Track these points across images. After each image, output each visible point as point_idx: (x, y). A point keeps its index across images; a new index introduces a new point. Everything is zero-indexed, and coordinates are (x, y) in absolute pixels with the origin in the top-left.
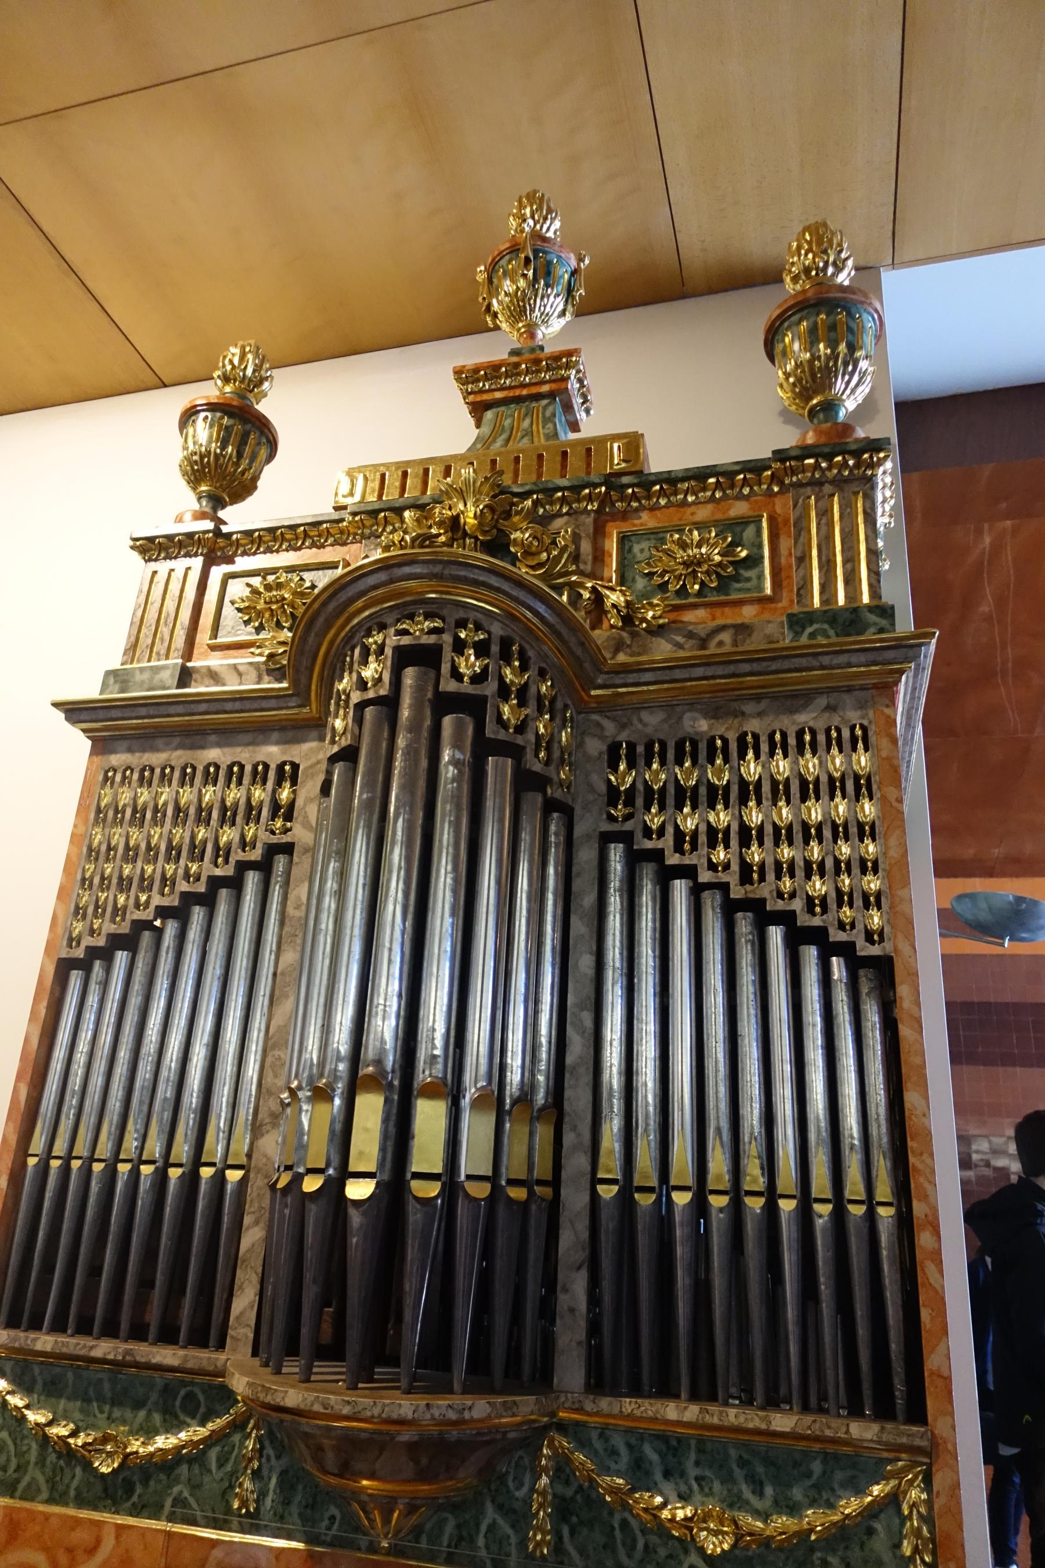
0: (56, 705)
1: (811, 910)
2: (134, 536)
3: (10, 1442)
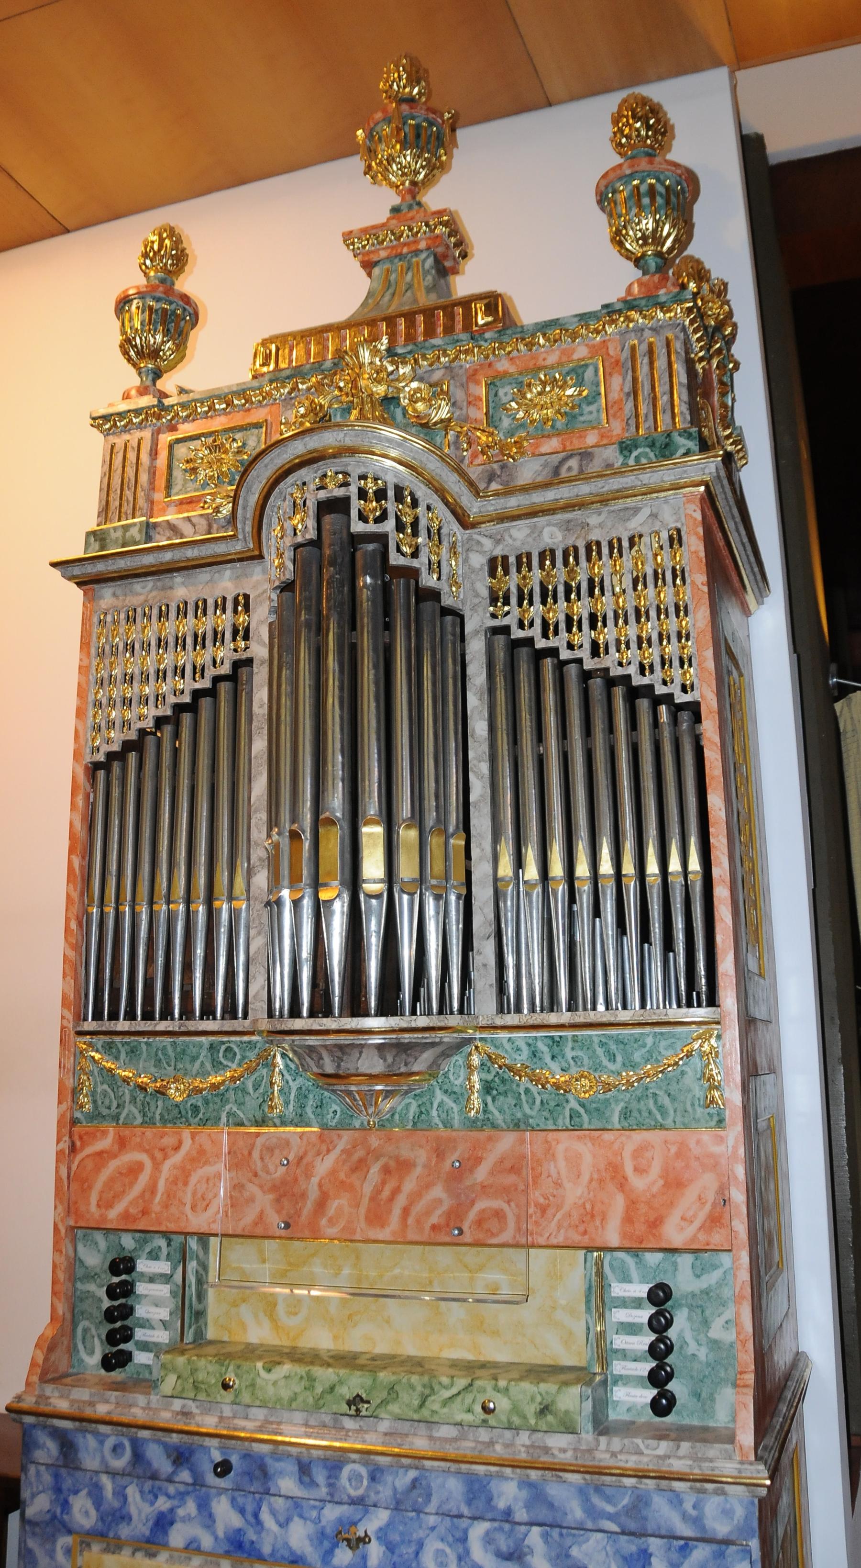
0: (54, 565)
1: (643, 673)
2: (95, 415)
3: (109, 1090)
